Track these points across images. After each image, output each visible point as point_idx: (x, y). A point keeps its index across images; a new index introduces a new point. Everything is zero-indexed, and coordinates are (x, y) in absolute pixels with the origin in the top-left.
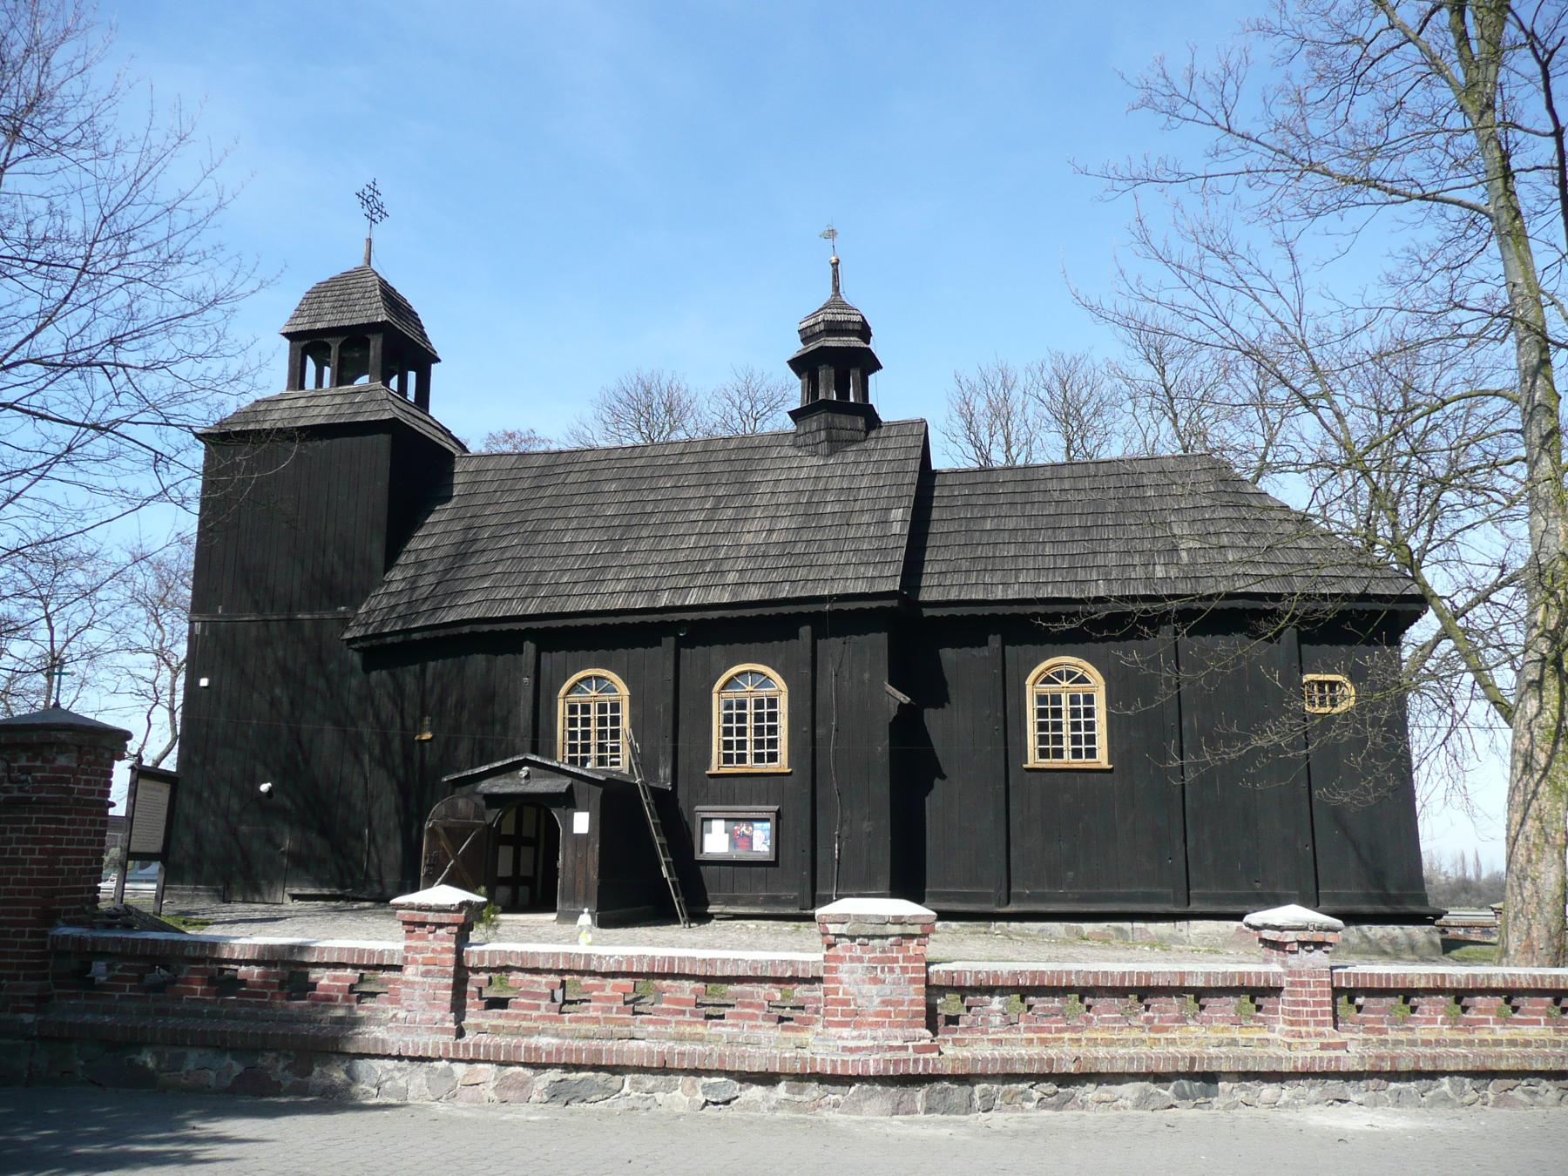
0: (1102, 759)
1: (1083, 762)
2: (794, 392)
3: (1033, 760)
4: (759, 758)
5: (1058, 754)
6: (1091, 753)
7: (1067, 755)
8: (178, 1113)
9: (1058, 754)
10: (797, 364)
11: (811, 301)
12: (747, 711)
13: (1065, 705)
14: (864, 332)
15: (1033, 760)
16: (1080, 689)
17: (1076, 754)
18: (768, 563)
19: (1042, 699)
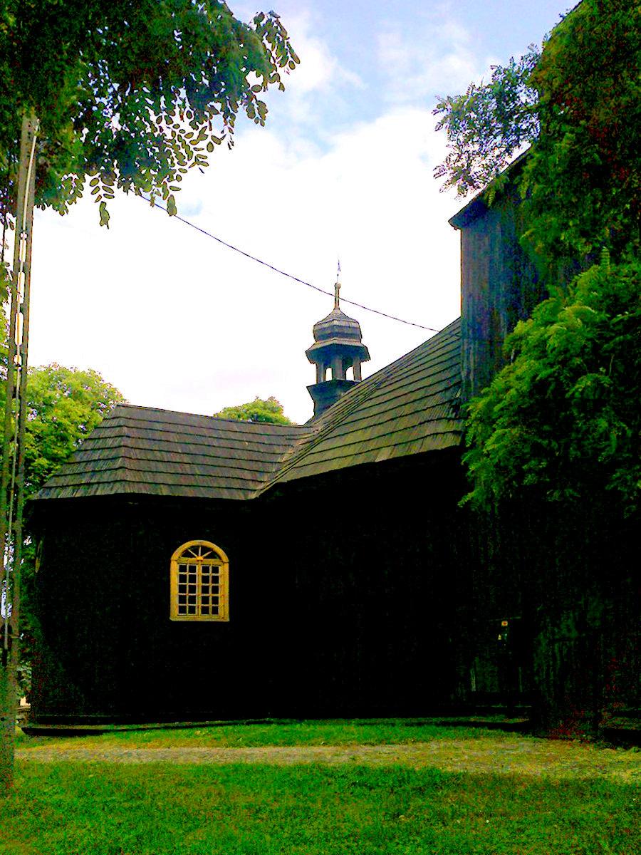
0: (224, 614)
1: (188, 617)
2: (309, 374)
3: (175, 616)
4: (205, 611)
5: (192, 610)
6: (215, 611)
7: (198, 611)
8: (526, 721)
9: (192, 610)
10: (313, 355)
11: (322, 309)
12: (196, 584)
13: (199, 572)
14: (357, 333)
15: (175, 616)
16: (212, 562)
17: (205, 611)
18: (90, 467)
19: (182, 568)
